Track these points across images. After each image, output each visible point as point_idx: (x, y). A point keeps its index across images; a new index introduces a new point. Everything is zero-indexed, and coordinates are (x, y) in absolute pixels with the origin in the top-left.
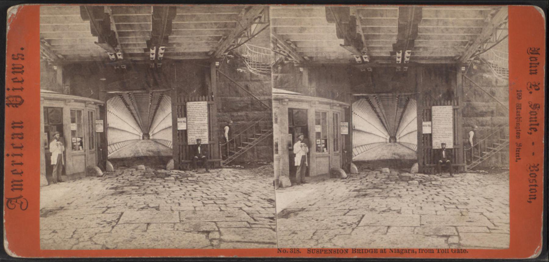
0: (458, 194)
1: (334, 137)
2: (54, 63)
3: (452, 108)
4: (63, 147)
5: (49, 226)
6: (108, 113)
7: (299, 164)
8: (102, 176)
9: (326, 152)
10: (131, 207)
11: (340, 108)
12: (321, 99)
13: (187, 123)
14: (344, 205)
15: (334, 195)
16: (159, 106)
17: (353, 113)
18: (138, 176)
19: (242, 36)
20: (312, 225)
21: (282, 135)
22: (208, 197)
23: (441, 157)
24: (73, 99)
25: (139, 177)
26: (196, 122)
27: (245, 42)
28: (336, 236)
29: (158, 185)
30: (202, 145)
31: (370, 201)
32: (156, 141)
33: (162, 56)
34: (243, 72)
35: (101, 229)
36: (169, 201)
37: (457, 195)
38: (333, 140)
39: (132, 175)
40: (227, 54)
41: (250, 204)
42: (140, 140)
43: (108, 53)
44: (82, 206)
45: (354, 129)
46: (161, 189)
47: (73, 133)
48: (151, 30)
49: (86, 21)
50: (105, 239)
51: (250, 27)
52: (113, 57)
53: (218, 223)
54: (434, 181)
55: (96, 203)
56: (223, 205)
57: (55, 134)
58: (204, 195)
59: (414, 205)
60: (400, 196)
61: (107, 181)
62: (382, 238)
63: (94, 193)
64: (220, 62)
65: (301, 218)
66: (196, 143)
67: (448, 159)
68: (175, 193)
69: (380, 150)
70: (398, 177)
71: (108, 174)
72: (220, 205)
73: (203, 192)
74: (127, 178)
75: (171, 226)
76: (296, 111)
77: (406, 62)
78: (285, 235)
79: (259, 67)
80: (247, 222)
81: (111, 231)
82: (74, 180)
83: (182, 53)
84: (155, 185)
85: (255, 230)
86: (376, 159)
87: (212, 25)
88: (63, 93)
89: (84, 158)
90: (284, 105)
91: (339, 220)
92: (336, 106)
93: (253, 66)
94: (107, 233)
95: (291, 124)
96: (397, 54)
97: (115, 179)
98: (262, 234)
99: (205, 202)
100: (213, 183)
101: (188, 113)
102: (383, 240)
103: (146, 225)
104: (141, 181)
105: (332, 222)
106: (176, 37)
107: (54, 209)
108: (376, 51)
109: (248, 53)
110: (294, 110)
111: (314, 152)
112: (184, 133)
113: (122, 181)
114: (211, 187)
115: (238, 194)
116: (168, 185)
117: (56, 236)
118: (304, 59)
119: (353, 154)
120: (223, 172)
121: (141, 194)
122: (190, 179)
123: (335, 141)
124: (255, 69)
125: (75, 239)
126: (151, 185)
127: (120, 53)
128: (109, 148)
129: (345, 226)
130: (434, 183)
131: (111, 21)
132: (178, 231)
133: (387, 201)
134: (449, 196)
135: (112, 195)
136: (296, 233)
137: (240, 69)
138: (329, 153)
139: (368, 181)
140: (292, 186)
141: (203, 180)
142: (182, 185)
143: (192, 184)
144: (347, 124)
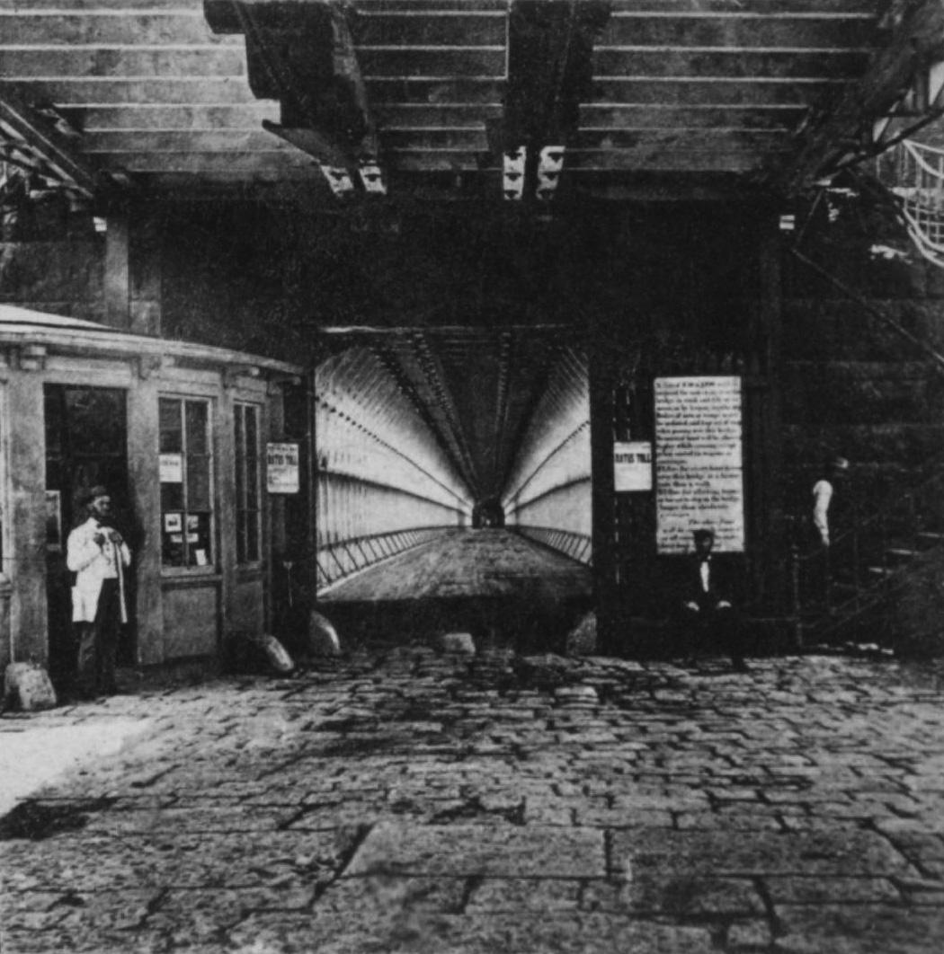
1: (239, 505)
3: (738, 388)
4: (125, 549)
5: (50, 875)
7: (90, 615)
8: (288, 674)
10: (402, 806)
11: (262, 386)
12: (178, 347)
15: (240, 746)
17: (318, 406)
18: (443, 677)
19: (892, 110)
21: (22, 494)
22: (734, 772)
24: (169, 355)
25: (448, 681)
26: (692, 462)
27: (905, 135)
28: (245, 914)
29: (527, 719)
34: (896, 256)
36: (568, 788)
38: (232, 518)
40: (827, 182)
42: (461, 528)
43: (326, 170)
44: (196, 798)
49: (228, 38)
51: (926, 76)
52: (347, 183)
53: (770, 883)
54: (662, 686)
55: (253, 786)
56: (793, 809)
57: (91, 498)
59: (579, 789)
61: (311, 694)
63: (250, 746)
65: (97, 840)
69: (433, 558)
72: (783, 809)
75: (571, 890)
76: (80, 395)
77: (546, 192)
78: (29, 910)
81: (312, 902)
83: (640, 172)
85: (924, 914)
86: (417, 596)
89: (213, 600)
90: (27, 371)
92: (246, 374)
93: (937, 235)
95: (57, 449)
96: (507, 161)
97: (345, 688)
101: (662, 424)
103: (460, 884)
106: (611, 110)
108: (416, 149)
110: (71, 394)
111: (152, 566)
112: (643, 505)
114: (751, 733)
115: (862, 761)
116: (566, 719)
117: (75, 918)
119: (320, 575)
120: (805, 671)
121: (450, 752)
122: (662, 694)
123: (244, 520)
126: (498, 718)
127: (376, 170)
128: (323, 559)
130: (662, 694)
131: (338, 40)
133: (464, 774)
134: (727, 750)
136: (79, 903)
138: (219, 570)
139: (383, 686)
140: (61, 702)
141: (717, 704)
142: (626, 718)
143: (669, 717)
144: (293, 449)
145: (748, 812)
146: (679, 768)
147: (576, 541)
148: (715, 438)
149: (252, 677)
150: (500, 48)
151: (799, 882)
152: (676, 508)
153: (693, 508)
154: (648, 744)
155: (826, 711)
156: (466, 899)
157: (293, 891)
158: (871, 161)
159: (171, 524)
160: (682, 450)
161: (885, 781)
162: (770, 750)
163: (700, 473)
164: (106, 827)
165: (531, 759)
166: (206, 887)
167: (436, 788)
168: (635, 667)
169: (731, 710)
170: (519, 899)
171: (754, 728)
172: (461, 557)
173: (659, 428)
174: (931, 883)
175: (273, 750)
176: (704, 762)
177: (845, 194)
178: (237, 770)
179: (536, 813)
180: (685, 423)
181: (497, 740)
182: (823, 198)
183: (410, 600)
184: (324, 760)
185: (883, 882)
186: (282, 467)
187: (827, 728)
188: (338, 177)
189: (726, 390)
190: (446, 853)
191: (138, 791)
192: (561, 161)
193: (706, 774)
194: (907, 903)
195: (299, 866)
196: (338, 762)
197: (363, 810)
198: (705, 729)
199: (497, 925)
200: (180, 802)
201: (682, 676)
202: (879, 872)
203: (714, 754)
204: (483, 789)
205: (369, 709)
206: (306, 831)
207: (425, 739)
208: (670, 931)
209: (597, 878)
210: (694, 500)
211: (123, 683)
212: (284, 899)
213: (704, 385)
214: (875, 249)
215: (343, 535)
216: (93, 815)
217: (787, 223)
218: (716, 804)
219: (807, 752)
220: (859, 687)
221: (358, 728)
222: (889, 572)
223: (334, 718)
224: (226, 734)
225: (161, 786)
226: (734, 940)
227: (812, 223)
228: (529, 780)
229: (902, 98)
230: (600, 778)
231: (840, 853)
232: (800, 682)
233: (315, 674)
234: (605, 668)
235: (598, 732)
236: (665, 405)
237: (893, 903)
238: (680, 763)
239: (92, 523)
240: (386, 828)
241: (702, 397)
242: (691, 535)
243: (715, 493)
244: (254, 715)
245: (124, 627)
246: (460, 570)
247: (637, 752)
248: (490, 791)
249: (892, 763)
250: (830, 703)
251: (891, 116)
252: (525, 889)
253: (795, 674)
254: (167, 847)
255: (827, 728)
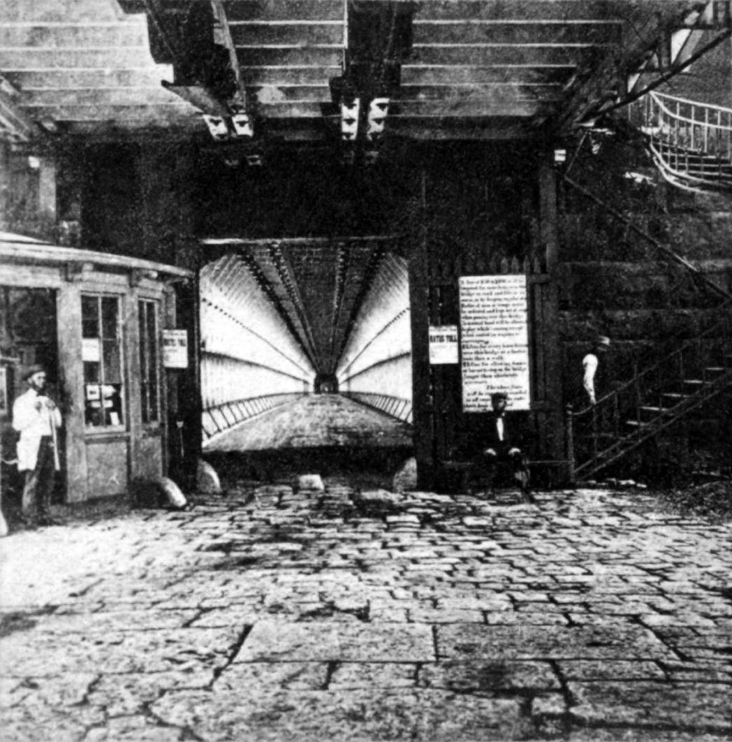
0: (552, 558)
2: (30, 147)
3: (524, 283)
6: (203, 306)
8: (182, 509)
9: (116, 425)
10: (276, 608)
11: (161, 287)
13: (459, 341)
14: (183, 596)
15: (148, 563)
16: (368, 288)
18: (300, 508)
19: (642, 67)
20: (83, 657)
22: (529, 580)
23: (492, 439)
24: (88, 262)
27: (652, 87)
28: (162, 692)
30: (509, 413)
31: (267, 582)
32: (353, 397)
33: (378, 128)
34: (644, 180)
35: (180, 677)
36: (401, 593)
37: (548, 558)
38: (137, 387)
39: (280, 506)
40: (591, 124)
41: (665, 605)
42: (306, 394)
43: (207, 118)
45: (205, 353)
46: (374, 550)
47: (91, 371)
48: (345, 44)
50: (191, 709)
52: (222, 128)
53: (562, 664)
55: (163, 595)
56: (576, 608)
58: (515, 574)
59: (411, 594)
60: (361, 566)
61: (200, 523)
62: (314, 701)
63: (155, 563)
64: (570, 151)
66: (490, 408)
67: (514, 445)
68: (421, 567)
70: (351, 503)
71: (203, 503)
72: (569, 607)
73: (511, 564)
74: (263, 514)
75: (409, 671)
77: (375, 135)
79: (698, 169)
80: (657, 661)
81: (211, 683)
82: (93, 519)
84: (355, 541)
85: (682, 688)
86: (276, 446)
87: (544, 32)
88: (58, 244)
91: (169, 641)
92: (147, 276)
94: (198, 689)
97: (226, 517)
98: (706, 701)
99: (519, 596)
100: (544, 537)
101: (465, 312)
102: (318, 705)
103: (325, 668)
104: (310, 525)
105: (146, 650)
106: (425, 70)
107: (29, 610)
109: (661, 122)
111: (77, 424)
112: (452, 375)
113: (249, 525)
114: (540, 550)
116: (396, 540)
118: (44, 130)
120: (578, 501)
121: (310, 566)
122: (470, 521)
123: (148, 389)
124: (683, 174)
125: (95, 708)
126: (343, 540)
127: (244, 118)
128: (206, 419)
129: (192, 662)
131: (216, 17)
132: (429, 690)
133: (321, 583)
134: (523, 563)
135: (217, 567)
137: (634, 175)
138: (128, 429)
139: (254, 516)
141: (512, 527)
142: (443, 539)
144: (182, 334)
145: (542, 611)
146: (487, 577)
147: (396, 403)
148: (507, 322)
149: (154, 511)
150: (339, 22)
151: (585, 664)
152: (477, 377)
153: (490, 376)
154: (436, 552)
155: (597, 533)
156: (329, 679)
157: (197, 674)
158: (624, 107)
159: (92, 393)
160: (481, 332)
161: (644, 586)
162: (555, 563)
163: (496, 350)
164: (51, 628)
165: (371, 572)
166: (130, 672)
167: (300, 593)
168: (445, 498)
169: (524, 532)
170: (370, 679)
171: (542, 546)
172: (307, 416)
173: (462, 315)
174: (688, 664)
175: (175, 566)
176: (505, 571)
177: (604, 133)
178: (148, 582)
179: (378, 612)
180: (484, 312)
181: (345, 557)
182: (588, 136)
183: (270, 449)
184: (214, 573)
185: (652, 664)
186: (175, 348)
187: (598, 546)
188: (217, 123)
189: (514, 287)
190: (312, 644)
191: (73, 600)
192: (386, 109)
193: (507, 582)
194: (668, 680)
195: (200, 655)
196: (226, 575)
197: (246, 612)
198: (504, 546)
199: (354, 699)
200: (106, 607)
201: (484, 506)
202: (648, 657)
203: (512, 565)
204: (337, 594)
205: (245, 533)
206: (204, 628)
207: (290, 556)
208: (487, 703)
209: (428, 662)
210: (491, 370)
211: (58, 517)
212: (189, 680)
213: (497, 282)
214: (628, 175)
215: (218, 402)
216: (41, 618)
217: (560, 156)
218: (516, 605)
219: (582, 563)
220: (621, 513)
221: (237, 548)
222: (642, 424)
223: (219, 541)
224: (137, 555)
225: (89, 596)
226: (538, 709)
227: (580, 156)
228: (371, 588)
229: (649, 58)
230: (426, 586)
231: (615, 642)
232: (576, 510)
233: (202, 508)
234: (424, 500)
235: (423, 550)
236: (468, 298)
237: (658, 681)
238: (488, 573)
239: (32, 393)
240: (265, 625)
241: (497, 291)
242: (488, 397)
243: (507, 364)
244: (157, 539)
245: (57, 473)
246: (307, 427)
247: (453, 565)
248: (343, 596)
249: (651, 572)
250: (600, 527)
251: (642, 72)
252: (374, 671)
253: (571, 504)
254: (99, 643)
255: (598, 546)
